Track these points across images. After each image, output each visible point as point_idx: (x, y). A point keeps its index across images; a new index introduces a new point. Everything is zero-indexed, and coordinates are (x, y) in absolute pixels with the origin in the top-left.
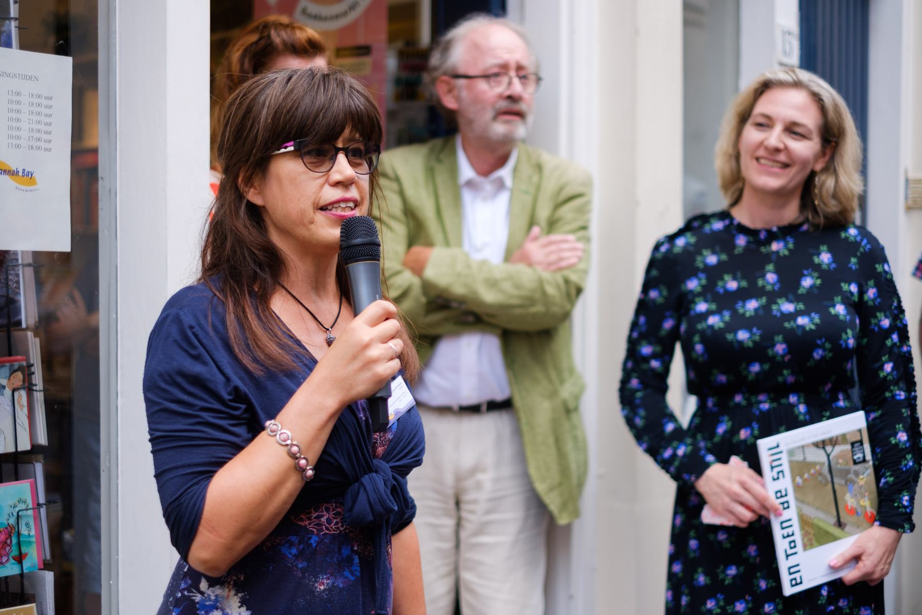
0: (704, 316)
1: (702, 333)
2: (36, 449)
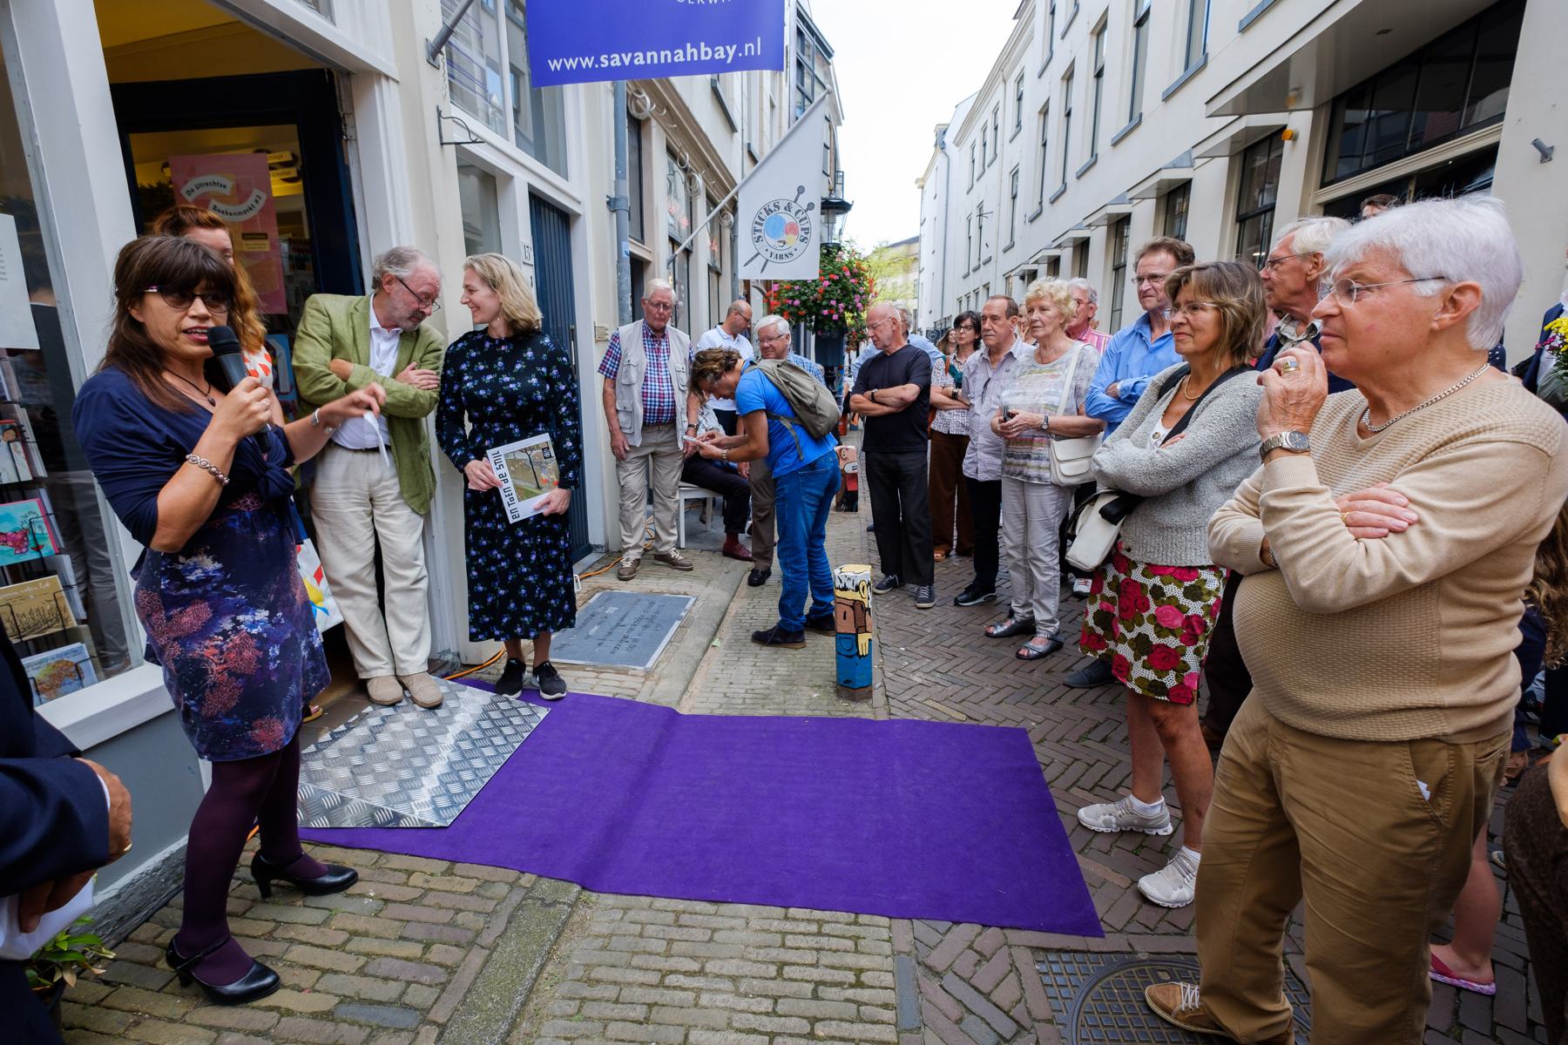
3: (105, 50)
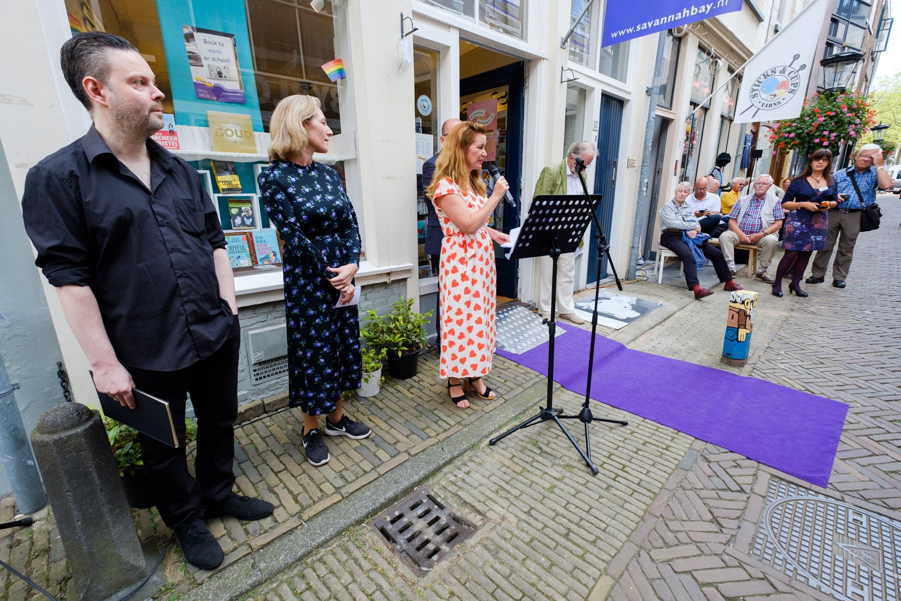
0: (304, 203)
1: (305, 210)
3: (461, 81)
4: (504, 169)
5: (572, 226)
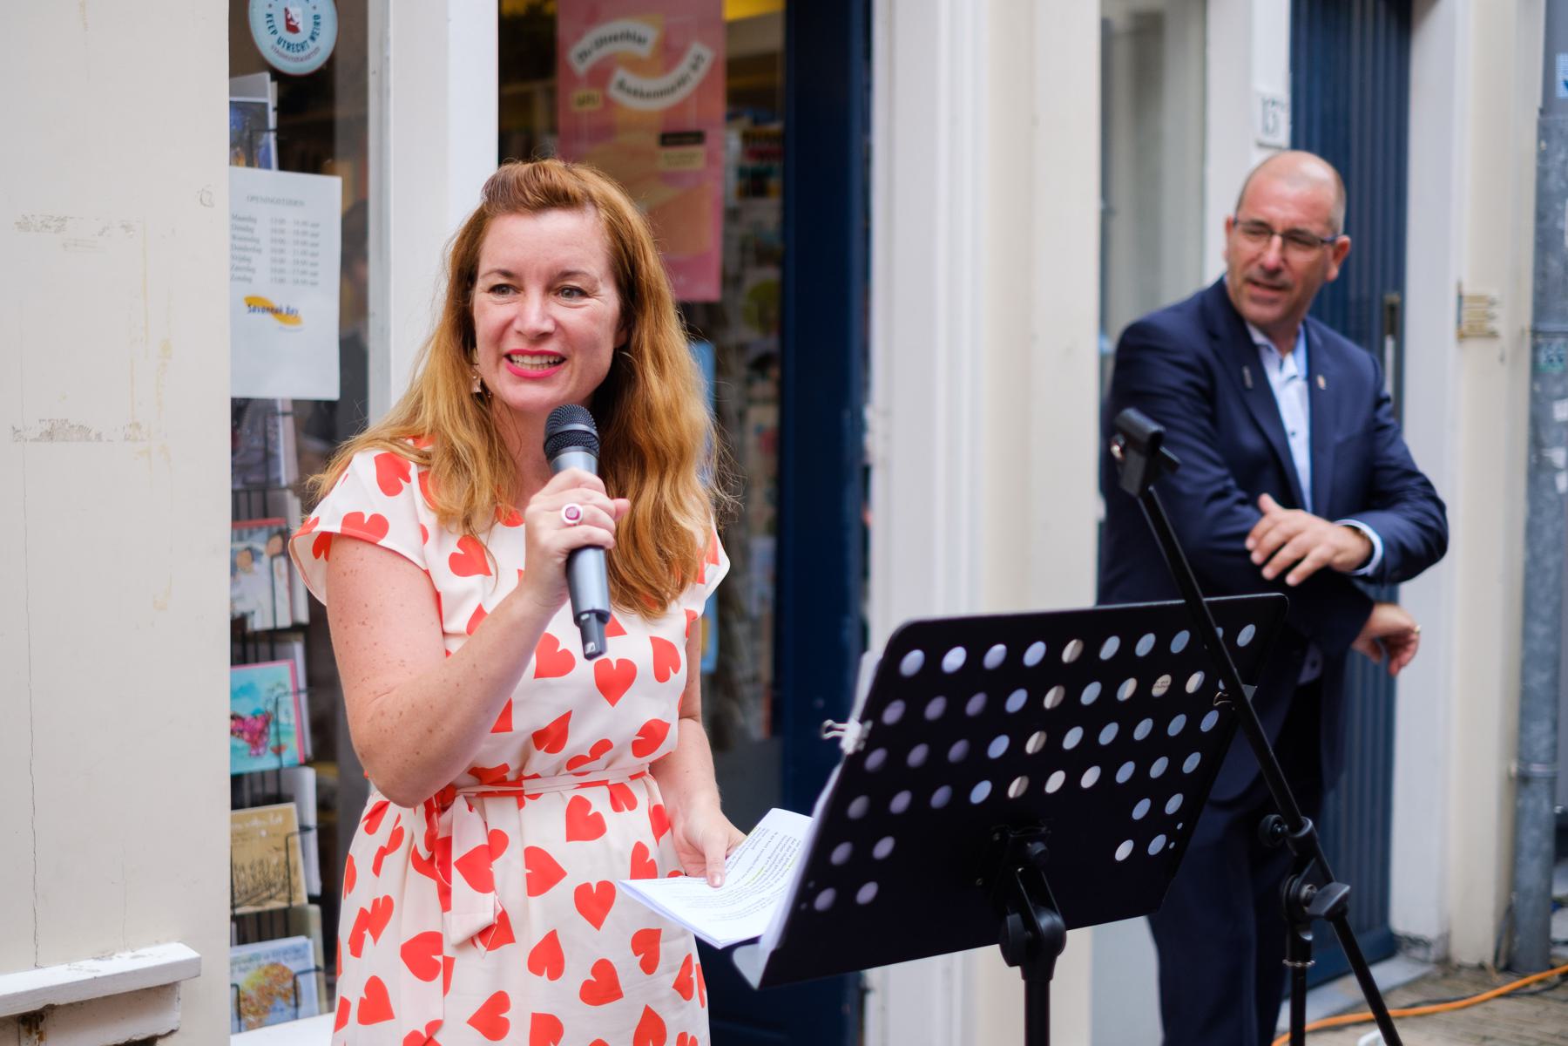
2: (296, 628)
4: (771, 344)
5: (1125, 773)
